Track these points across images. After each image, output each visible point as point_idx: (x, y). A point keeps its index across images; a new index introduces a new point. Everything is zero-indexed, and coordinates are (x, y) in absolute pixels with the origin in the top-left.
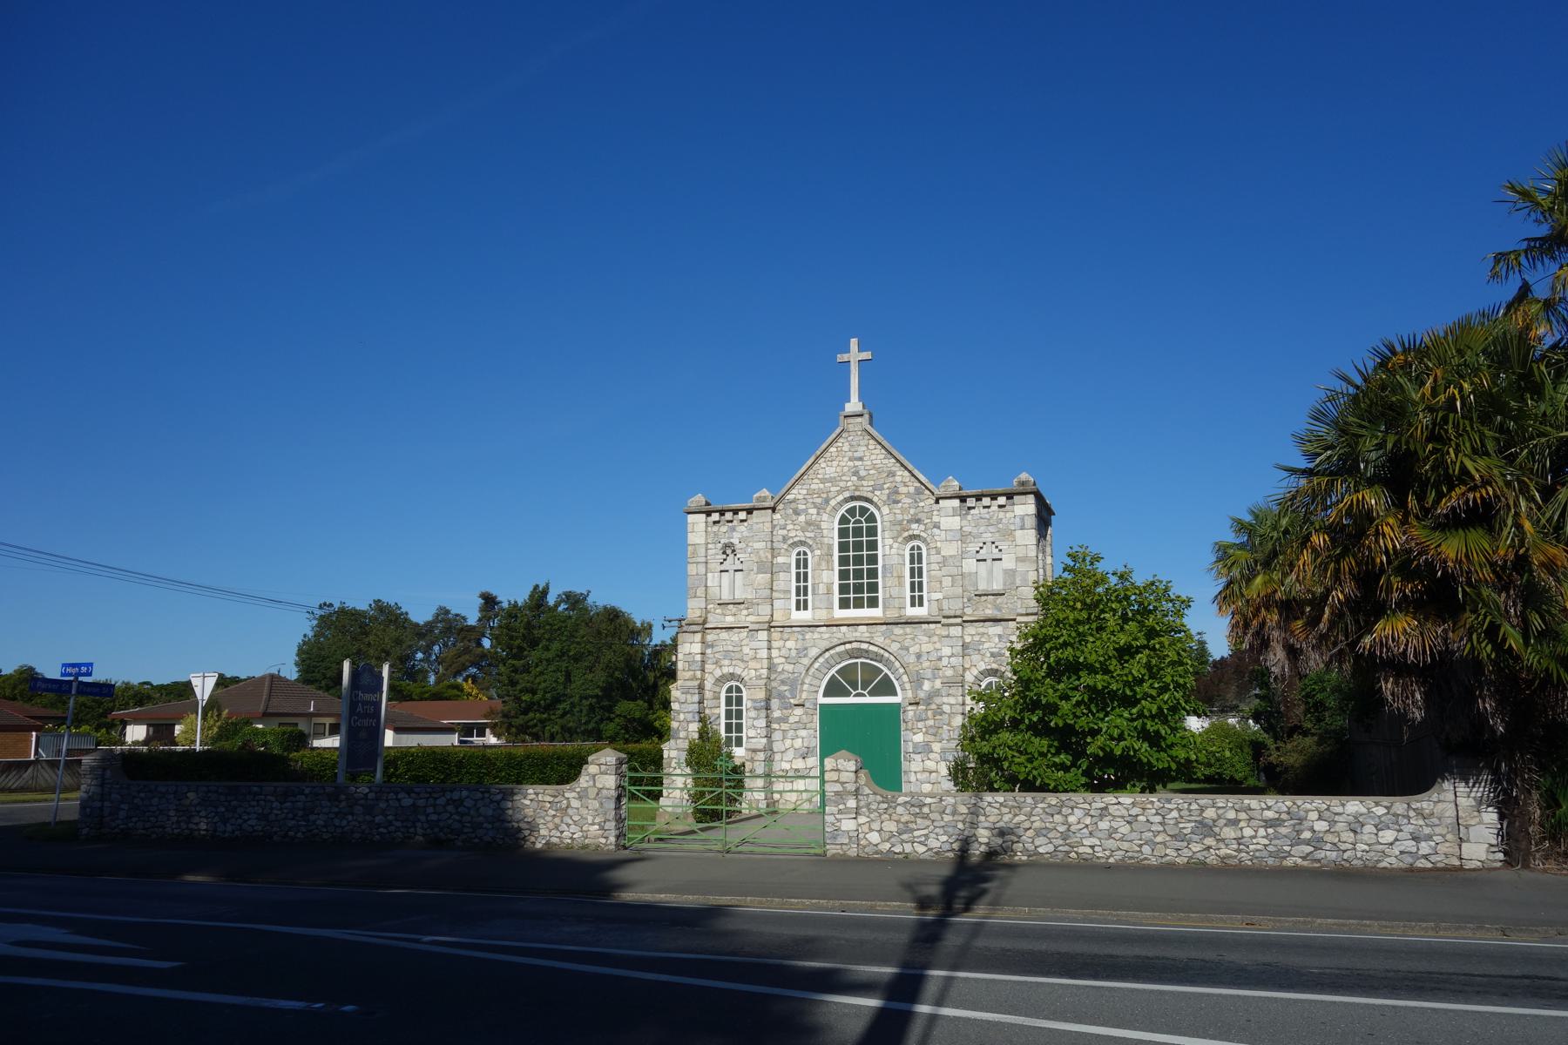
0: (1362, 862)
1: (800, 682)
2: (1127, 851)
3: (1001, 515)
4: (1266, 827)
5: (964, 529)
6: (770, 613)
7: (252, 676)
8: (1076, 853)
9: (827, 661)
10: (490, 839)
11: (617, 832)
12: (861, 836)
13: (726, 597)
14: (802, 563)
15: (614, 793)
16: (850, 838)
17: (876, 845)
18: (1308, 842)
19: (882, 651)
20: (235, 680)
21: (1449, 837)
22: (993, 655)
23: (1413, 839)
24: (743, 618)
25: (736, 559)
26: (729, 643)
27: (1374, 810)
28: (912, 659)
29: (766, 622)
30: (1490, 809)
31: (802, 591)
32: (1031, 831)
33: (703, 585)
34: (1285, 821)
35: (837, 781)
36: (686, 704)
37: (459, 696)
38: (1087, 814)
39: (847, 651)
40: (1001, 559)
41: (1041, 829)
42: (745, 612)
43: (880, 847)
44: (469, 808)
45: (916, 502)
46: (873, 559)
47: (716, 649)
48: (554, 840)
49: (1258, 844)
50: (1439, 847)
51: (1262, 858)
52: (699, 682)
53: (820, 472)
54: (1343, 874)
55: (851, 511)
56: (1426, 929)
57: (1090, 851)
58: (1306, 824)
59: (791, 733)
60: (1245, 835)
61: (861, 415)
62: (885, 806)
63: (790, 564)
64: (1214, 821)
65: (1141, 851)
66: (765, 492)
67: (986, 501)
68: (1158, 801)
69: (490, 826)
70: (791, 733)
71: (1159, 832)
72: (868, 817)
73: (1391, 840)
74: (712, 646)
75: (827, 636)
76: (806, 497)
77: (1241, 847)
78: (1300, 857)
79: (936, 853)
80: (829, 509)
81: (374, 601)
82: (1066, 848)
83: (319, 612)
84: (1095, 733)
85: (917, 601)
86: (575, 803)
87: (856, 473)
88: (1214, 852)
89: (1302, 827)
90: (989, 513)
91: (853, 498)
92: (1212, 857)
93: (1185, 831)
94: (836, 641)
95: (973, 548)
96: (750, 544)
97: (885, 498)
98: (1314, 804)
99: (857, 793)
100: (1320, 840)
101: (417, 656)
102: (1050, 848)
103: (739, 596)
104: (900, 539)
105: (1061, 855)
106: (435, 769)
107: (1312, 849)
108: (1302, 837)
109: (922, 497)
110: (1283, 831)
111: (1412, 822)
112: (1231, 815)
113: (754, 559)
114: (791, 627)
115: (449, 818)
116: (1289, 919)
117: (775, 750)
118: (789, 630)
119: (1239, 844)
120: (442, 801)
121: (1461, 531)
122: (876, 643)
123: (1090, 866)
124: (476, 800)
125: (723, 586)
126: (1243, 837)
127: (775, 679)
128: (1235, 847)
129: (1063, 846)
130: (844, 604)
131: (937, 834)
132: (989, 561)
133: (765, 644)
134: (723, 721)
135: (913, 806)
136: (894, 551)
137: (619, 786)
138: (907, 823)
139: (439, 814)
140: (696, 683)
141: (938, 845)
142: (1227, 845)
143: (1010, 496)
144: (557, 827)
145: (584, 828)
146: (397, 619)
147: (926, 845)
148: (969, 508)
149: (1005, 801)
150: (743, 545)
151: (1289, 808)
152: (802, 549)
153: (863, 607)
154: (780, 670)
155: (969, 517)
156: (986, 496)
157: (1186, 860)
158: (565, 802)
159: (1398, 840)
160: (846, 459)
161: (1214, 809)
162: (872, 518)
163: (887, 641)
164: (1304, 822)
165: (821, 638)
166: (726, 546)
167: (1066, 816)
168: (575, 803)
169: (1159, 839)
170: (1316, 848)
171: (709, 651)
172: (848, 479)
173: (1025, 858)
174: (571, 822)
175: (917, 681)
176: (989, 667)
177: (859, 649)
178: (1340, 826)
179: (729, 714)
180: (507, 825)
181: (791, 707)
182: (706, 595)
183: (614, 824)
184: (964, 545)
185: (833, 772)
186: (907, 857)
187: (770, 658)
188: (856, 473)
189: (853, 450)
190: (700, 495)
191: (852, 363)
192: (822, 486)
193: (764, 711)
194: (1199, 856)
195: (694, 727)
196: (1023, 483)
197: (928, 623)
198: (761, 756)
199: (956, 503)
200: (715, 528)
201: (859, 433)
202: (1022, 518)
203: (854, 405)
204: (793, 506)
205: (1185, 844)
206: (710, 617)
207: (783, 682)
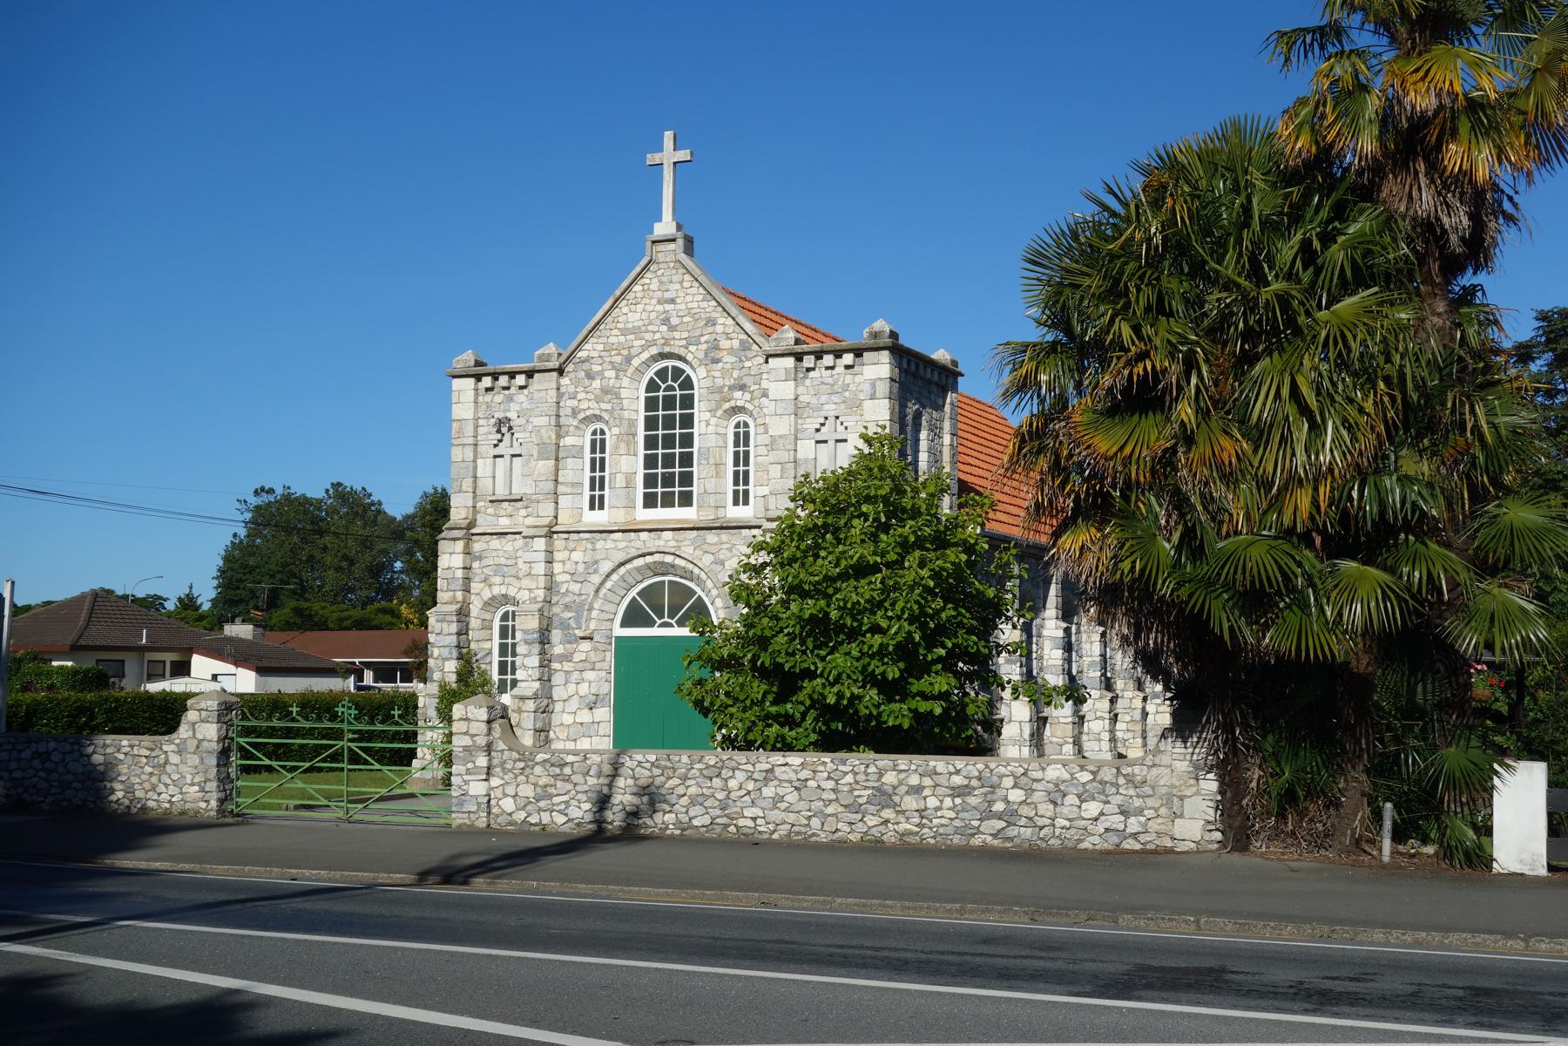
0: (1060, 842)
1: (587, 607)
2: (793, 825)
3: (848, 379)
4: (953, 796)
5: (800, 398)
6: (552, 514)
7: (152, 594)
8: (735, 825)
9: (623, 578)
10: (80, 803)
11: (222, 795)
12: (493, 802)
13: (501, 492)
14: (598, 445)
15: (215, 746)
16: (479, 804)
17: (510, 814)
18: (999, 816)
19: (690, 566)
20: (28, 608)
21: (1163, 811)
23: (1122, 813)
24: (521, 519)
25: (514, 440)
26: (501, 553)
27: (1077, 775)
29: (546, 526)
30: (1211, 776)
31: (597, 484)
32: (686, 798)
33: (471, 474)
34: (975, 789)
35: (465, 733)
36: (441, 636)
37: (392, 624)
38: (749, 778)
39: (648, 566)
40: (846, 441)
41: (697, 796)
42: (523, 512)
43: (515, 816)
44: (56, 763)
45: (741, 361)
46: (687, 440)
47: (485, 562)
48: (151, 804)
49: (942, 817)
50: (1150, 823)
51: (946, 835)
52: (458, 606)
53: (620, 319)
54: (1031, 856)
55: (662, 374)
56: (950, 911)
57: (751, 824)
58: (1000, 793)
59: (576, 675)
60: (929, 805)
61: (673, 240)
62: (522, 765)
63: (582, 447)
64: (895, 788)
65: (808, 825)
66: (551, 348)
67: (828, 360)
68: (832, 762)
69: (79, 786)
70: (576, 675)
71: (831, 801)
72: (503, 779)
73: (1095, 813)
74: (480, 558)
75: (623, 545)
76: (603, 354)
77: (924, 821)
78: (991, 835)
79: (578, 825)
80: (631, 370)
81: (332, 484)
83: (254, 501)
84: (810, 675)
85: (741, 498)
86: (174, 759)
87: (666, 321)
88: (896, 826)
89: (995, 797)
90: (832, 376)
91: (663, 356)
92: (890, 833)
93: (860, 801)
94: (634, 553)
95: (812, 424)
96: (531, 420)
97: (701, 355)
98: (1009, 768)
99: (489, 748)
100: (1015, 813)
101: (396, 565)
102: (707, 820)
103: (517, 490)
104: (719, 413)
105: (718, 829)
106: (151, 719)
107: (1004, 824)
108: (994, 809)
109: (750, 354)
110: (973, 801)
111: (1121, 791)
112: (914, 780)
113: (534, 439)
114: (579, 532)
115: (35, 776)
116: (807, 898)
117: (555, 697)
118: (575, 536)
119: (922, 818)
120: (26, 754)
121: (1151, 414)
122: (683, 555)
123: (752, 843)
124: (64, 754)
125: (494, 476)
126: (926, 809)
127: (558, 603)
128: (917, 820)
129: (722, 817)
130: (650, 502)
131: (579, 801)
132: (831, 443)
133: (542, 556)
134: (496, 658)
135: (552, 765)
136: (711, 429)
137: (226, 738)
138: (545, 786)
139: (24, 770)
140: (455, 607)
141: (580, 814)
142: (908, 819)
143: (858, 353)
144: (154, 788)
145: (184, 790)
146: (365, 511)
147: (566, 815)
148: (808, 370)
149: (657, 760)
150: (522, 421)
151: (980, 773)
152: (598, 426)
153: (674, 506)
154: (563, 590)
155: (808, 382)
156: (828, 352)
157: (859, 836)
158: (163, 756)
159: (1104, 814)
160: (654, 301)
161: (895, 773)
162: (688, 384)
163: (698, 552)
164: (997, 790)
165: (615, 548)
166: (500, 422)
168: (174, 759)
169: (830, 810)
170: (1009, 824)
171: (476, 565)
172: (656, 329)
173: (677, 832)
174: (169, 781)
177: (663, 563)
178: (1038, 796)
179: (503, 650)
180: (99, 784)
181: (576, 641)
182: (475, 488)
183: (215, 784)
184: (800, 421)
185: (462, 722)
186: (543, 829)
187: (550, 575)
188: (666, 321)
189: (663, 288)
190: (551, 344)
191: (665, 166)
192: (622, 339)
193: (537, 645)
194: (874, 831)
195: (451, 666)
196: (875, 335)
197: (750, 527)
198: (531, 705)
199: (790, 362)
200: (488, 397)
201: (672, 265)
202: (873, 384)
203: (665, 226)
204: (586, 366)
205: (859, 816)
206: (480, 519)
207: (567, 607)
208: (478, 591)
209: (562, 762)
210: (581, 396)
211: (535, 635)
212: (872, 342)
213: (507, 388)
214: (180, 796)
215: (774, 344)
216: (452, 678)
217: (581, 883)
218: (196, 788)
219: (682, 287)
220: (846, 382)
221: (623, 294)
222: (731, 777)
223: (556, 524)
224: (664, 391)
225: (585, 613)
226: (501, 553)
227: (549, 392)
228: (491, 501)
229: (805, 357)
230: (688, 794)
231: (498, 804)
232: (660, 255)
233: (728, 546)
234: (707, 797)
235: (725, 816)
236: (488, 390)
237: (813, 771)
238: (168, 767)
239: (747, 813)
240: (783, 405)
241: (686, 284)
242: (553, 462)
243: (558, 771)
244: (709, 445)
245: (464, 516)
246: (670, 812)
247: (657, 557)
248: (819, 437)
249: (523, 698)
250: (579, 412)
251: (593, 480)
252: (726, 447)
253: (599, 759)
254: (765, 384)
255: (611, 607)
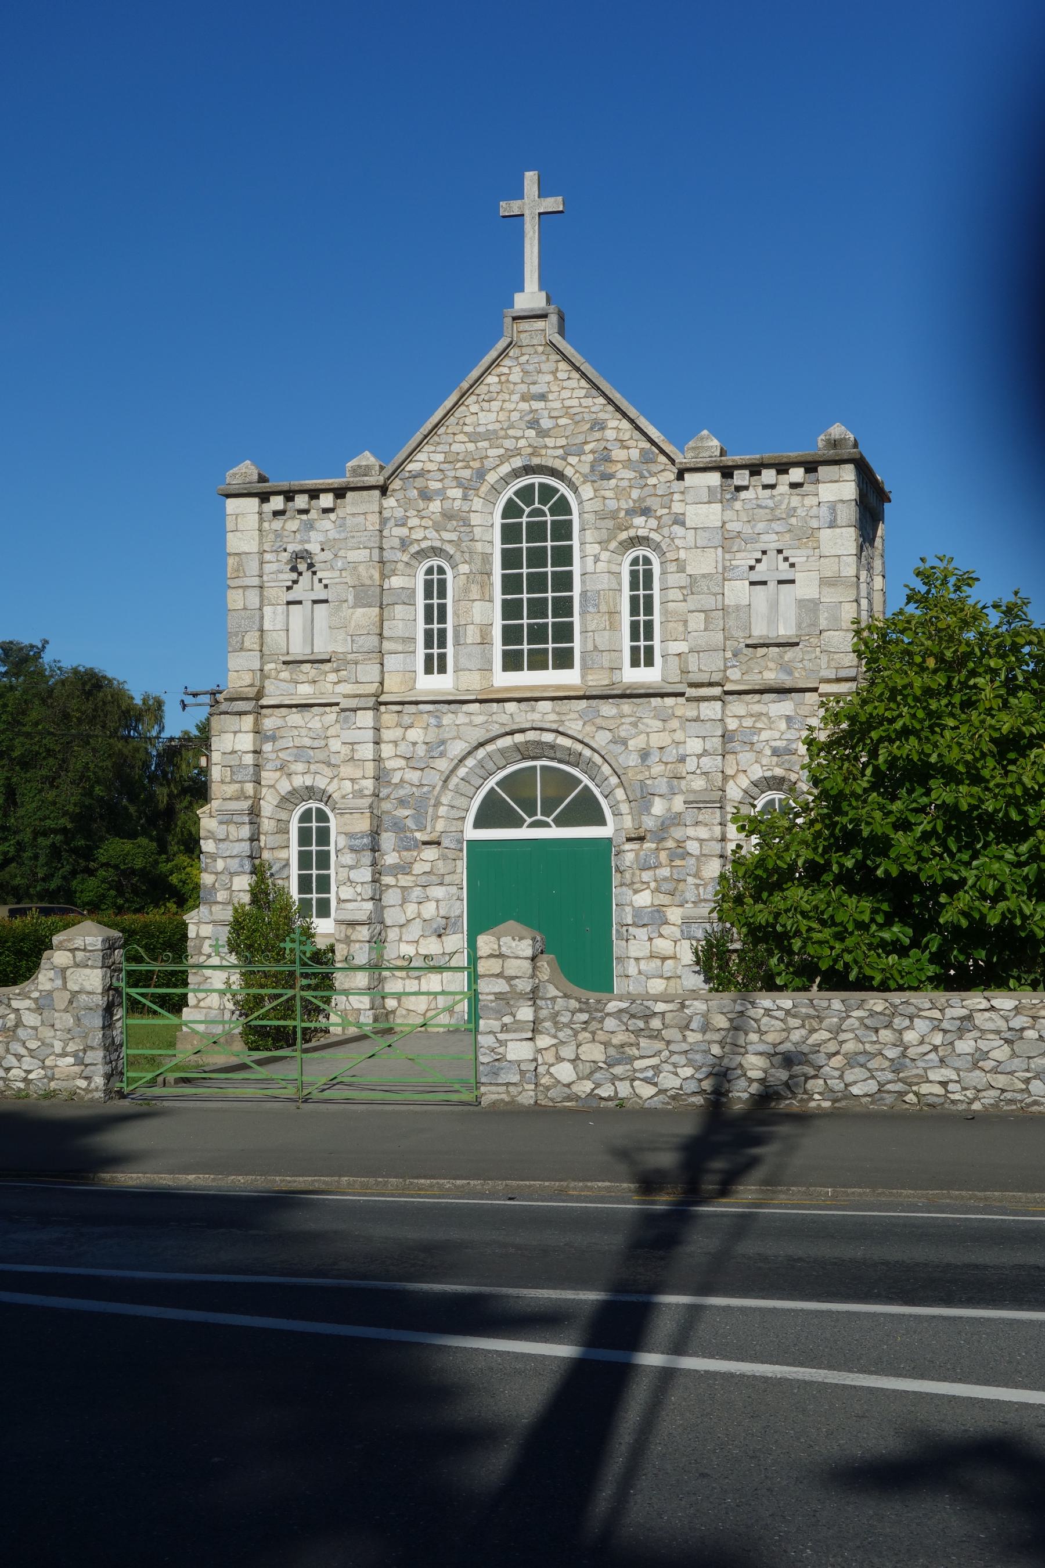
1: (432, 802)
2: (1003, 1091)
3: (795, 501)
5: (728, 526)
6: (378, 679)
8: (916, 1094)
9: (481, 764)
11: (108, 1068)
12: (541, 1069)
13: (298, 649)
14: (436, 588)
15: (100, 1001)
16: (522, 1073)
17: (568, 1085)
19: (579, 747)
22: (775, 752)
24: (329, 686)
25: (316, 580)
26: (304, 732)
28: (633, 760)
31: (435, 639)
32: (839, 1057)
33: (256, 627)
39: (517, 747)
40: (793, 582)
41: (856, 1054)
42: (332, 677)
43: (575, 1088)
45: (642, 477)
46: (564, 582)
47: (281, 744)
52: (250, 802)
53: (468, 421)
55: (525, 493)
57: (940, 1090)
59: (417, 892)
61: (544, 316)
62: (584, 1017)
63: (414, 590)
65: (1027, 1091)
66: (367, 459)
67: (768, 476)
70: (417, 892)
72: (555, 1037)
74: (273, 739)
76: (442, 466)
79: (674, 1098)
82: (899, 1087)
85: (642, 657)
86: (31, 1019)
87: (534, 424)
90: (772, 497)
91: (528, 470)
94: (496, 729)
95: (744, 560)
97: (586, 469)
102: (872, 1087)
103: (322, 648)
104: (613, 545)
105: (889, 1099)
109: (654, 468)
113: (348, 580)
114: (417, 703)
118: (412, 708)
122: (569, 732)
127: (388, 797)
130: (512, 662)
132: (308, 604)
133: (369, 735)
134: (294, 871)
135: (633, 1016)
136: (601, 566)
137: (110, 988)
138: (622, 1046)
140: (246, 805)
141: (677, 1083)
143: (811, 467)
145: (48, 1063)
147: (655, 1084)
148: (739, 489)
150: (328, 555)
152: (435, 562)
153: (522, 669)
154: (396, 780)
155: (738, 505)
158: (12, 1016)
160: (516, 397)
162: (562, 507)
163: (589, 728)
165: (470, 723)
166: (298, 556)
167: (900, 1032)
168: (31, 1019)
171: (267, 747)
172: (519, 433)
173: (827, 1104)
175: (642, 800)
176: (768, 774)
177: (539, 743)
179: (304, 860)
181: (416, 847)
183: (100, 1054)
184: (727, 556)
185: (493, 960)
186: (621, 1106)
187: (378, 760)
188: (534, 424)
190: (367, 453)
191: (527, 218)
192: (471, 447)
193: (369, 853)
195: (243, 883)
196: (835, 444)
198: (364, 933)
199: (714, 479)
200: (277, 524)
202: (833, 507)
204: (419, 482)
206: (270, 687)
207: (402, 802)
208: (272, 783)
209: (648, 1013)
210: (413, 522)
211: (365, 840)
212: (831, 453)
213: (306, 512)
214: (43, 1072)
215: (690, 454)
216: (246, 898)
217: (903, 1188)
218: (70, 1060)
219: (556, 378)
220: (793, 505)
221: (471, 386)
222: (907, 1028)
223: (382, 692)
224: (528, 516)
225: (430, 810)
226: (304, 732)
227: (370, 517)
228: (284, 663)
229: (736, 472)
230: (842, 1051)
231: (548, 1072)
232: (523, 336)
233: (633, 719)
234: (873, 1056)
235: (899, 1080)
236: (277, 514)
237: (1033, 1017)
238: (20, 1032)
239: (933, 1076)
240: (706, 534)
241: (561, 375)
242: (377, 609)
243: (641, 1024)
244: (600, 587)
245: (248, 682)
246: (815, 1077)
247: (531, 736)
248: (755, 577)
249: (352, 924)
250: (411, 543)
251: (428, 634)
252: (620, 590)
253: (704, 1007)
254: (677, 508)
255: (461, 802)
